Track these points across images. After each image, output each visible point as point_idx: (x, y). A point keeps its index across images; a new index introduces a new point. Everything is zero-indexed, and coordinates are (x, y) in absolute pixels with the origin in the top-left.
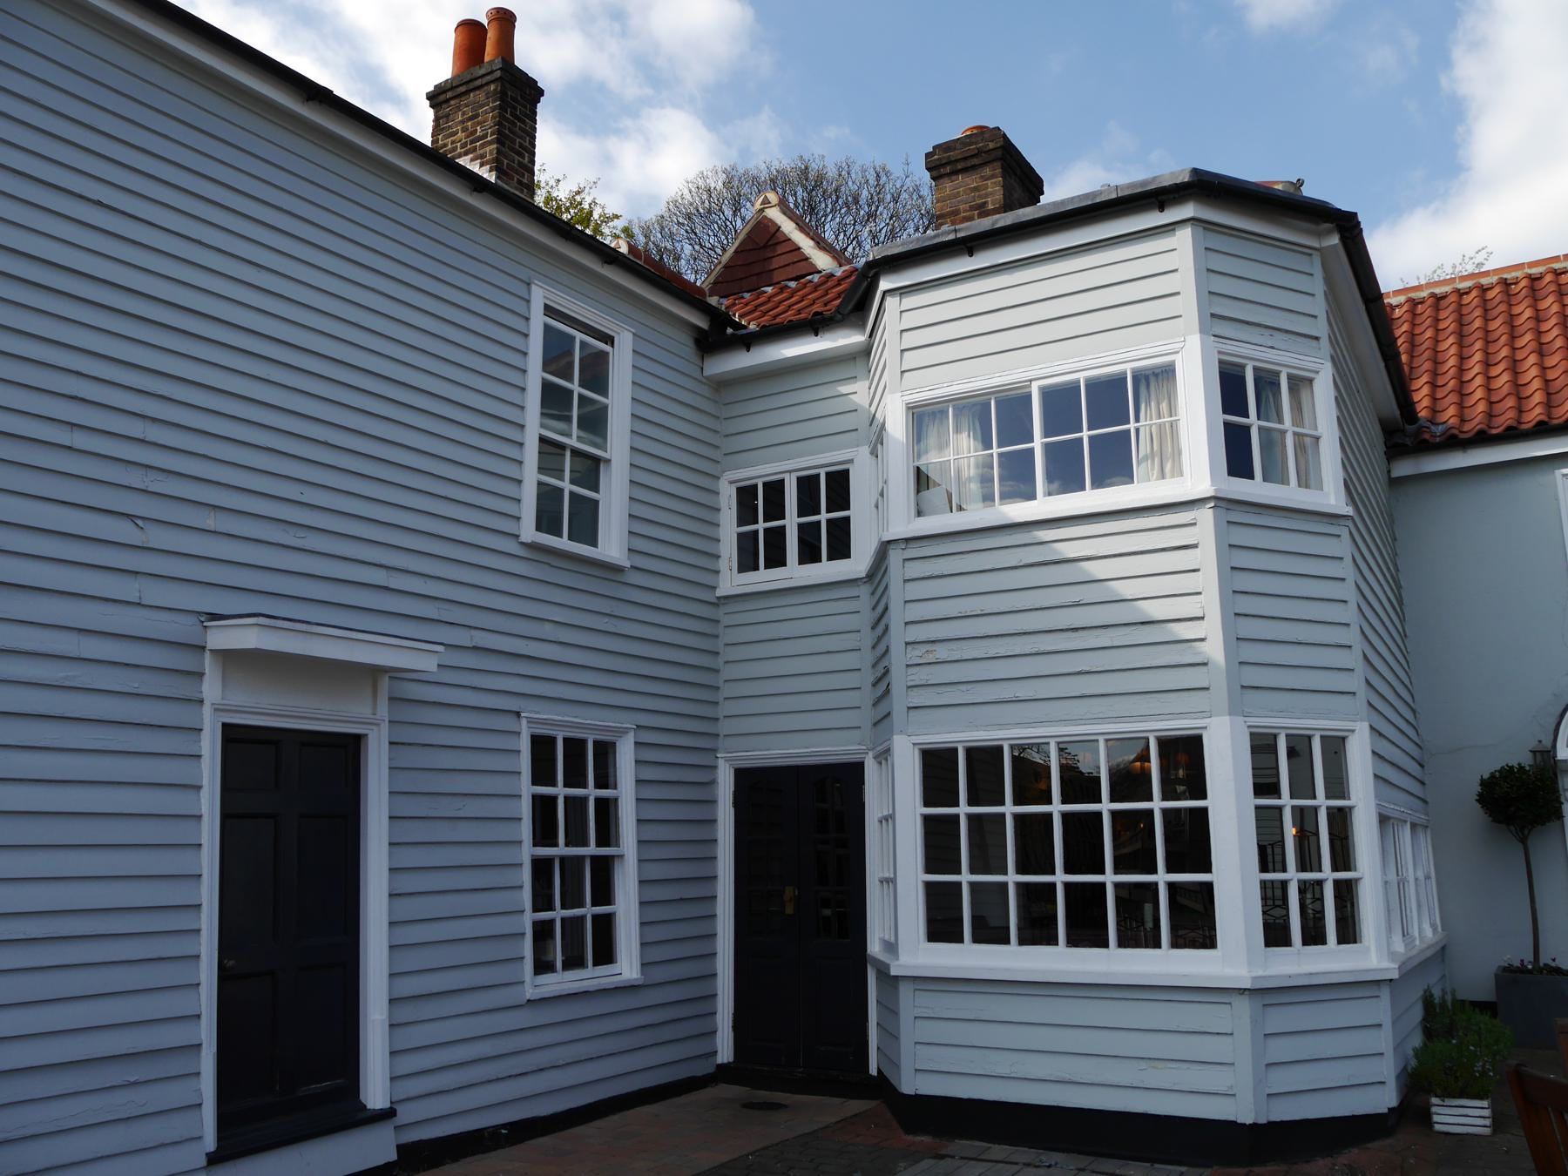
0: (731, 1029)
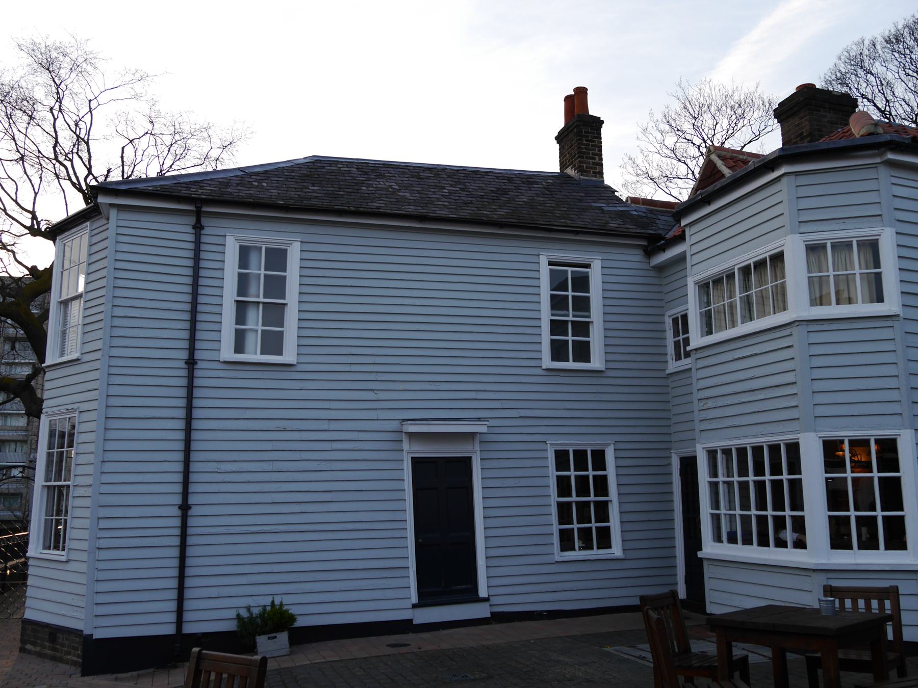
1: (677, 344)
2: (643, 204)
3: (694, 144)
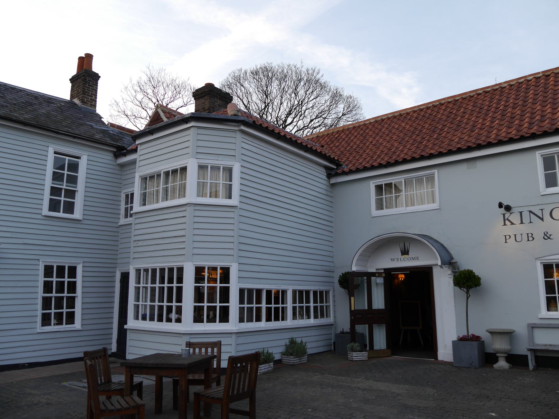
0: (116, 343)
1: (126, 209)
2: (117, 128)
3: (152, 102)
